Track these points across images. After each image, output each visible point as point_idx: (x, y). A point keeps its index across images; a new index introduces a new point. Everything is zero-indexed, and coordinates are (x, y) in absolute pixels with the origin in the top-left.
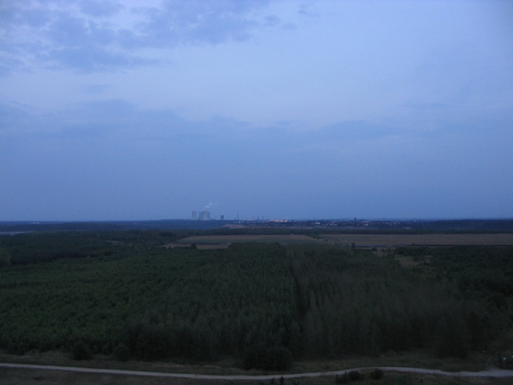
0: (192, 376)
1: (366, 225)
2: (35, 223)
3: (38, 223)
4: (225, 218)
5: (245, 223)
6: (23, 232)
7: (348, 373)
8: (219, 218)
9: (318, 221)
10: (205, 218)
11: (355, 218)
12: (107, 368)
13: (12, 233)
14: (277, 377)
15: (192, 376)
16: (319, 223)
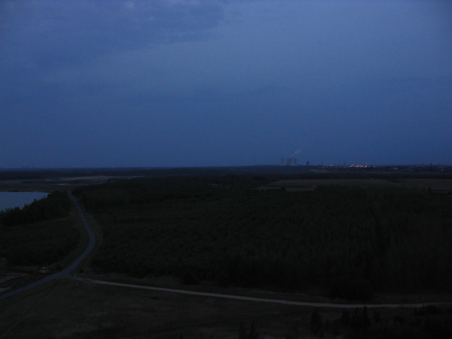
0: (284, 302)
1: (442, 170)
2: (147, 169)
3: (150, 169)
4: (311, 164)
5: (329, 168)
6: (138, 177)
7: (4, 212)
8: (305, 164)
9: (396, 167)
10: (293, 164)
11: (6, 209)
12: (211, 292)
13: (129, 178)
14: (362, 306)
15: (284, 302)
16: (396, 169)
